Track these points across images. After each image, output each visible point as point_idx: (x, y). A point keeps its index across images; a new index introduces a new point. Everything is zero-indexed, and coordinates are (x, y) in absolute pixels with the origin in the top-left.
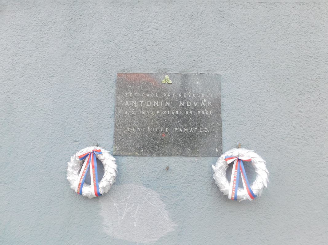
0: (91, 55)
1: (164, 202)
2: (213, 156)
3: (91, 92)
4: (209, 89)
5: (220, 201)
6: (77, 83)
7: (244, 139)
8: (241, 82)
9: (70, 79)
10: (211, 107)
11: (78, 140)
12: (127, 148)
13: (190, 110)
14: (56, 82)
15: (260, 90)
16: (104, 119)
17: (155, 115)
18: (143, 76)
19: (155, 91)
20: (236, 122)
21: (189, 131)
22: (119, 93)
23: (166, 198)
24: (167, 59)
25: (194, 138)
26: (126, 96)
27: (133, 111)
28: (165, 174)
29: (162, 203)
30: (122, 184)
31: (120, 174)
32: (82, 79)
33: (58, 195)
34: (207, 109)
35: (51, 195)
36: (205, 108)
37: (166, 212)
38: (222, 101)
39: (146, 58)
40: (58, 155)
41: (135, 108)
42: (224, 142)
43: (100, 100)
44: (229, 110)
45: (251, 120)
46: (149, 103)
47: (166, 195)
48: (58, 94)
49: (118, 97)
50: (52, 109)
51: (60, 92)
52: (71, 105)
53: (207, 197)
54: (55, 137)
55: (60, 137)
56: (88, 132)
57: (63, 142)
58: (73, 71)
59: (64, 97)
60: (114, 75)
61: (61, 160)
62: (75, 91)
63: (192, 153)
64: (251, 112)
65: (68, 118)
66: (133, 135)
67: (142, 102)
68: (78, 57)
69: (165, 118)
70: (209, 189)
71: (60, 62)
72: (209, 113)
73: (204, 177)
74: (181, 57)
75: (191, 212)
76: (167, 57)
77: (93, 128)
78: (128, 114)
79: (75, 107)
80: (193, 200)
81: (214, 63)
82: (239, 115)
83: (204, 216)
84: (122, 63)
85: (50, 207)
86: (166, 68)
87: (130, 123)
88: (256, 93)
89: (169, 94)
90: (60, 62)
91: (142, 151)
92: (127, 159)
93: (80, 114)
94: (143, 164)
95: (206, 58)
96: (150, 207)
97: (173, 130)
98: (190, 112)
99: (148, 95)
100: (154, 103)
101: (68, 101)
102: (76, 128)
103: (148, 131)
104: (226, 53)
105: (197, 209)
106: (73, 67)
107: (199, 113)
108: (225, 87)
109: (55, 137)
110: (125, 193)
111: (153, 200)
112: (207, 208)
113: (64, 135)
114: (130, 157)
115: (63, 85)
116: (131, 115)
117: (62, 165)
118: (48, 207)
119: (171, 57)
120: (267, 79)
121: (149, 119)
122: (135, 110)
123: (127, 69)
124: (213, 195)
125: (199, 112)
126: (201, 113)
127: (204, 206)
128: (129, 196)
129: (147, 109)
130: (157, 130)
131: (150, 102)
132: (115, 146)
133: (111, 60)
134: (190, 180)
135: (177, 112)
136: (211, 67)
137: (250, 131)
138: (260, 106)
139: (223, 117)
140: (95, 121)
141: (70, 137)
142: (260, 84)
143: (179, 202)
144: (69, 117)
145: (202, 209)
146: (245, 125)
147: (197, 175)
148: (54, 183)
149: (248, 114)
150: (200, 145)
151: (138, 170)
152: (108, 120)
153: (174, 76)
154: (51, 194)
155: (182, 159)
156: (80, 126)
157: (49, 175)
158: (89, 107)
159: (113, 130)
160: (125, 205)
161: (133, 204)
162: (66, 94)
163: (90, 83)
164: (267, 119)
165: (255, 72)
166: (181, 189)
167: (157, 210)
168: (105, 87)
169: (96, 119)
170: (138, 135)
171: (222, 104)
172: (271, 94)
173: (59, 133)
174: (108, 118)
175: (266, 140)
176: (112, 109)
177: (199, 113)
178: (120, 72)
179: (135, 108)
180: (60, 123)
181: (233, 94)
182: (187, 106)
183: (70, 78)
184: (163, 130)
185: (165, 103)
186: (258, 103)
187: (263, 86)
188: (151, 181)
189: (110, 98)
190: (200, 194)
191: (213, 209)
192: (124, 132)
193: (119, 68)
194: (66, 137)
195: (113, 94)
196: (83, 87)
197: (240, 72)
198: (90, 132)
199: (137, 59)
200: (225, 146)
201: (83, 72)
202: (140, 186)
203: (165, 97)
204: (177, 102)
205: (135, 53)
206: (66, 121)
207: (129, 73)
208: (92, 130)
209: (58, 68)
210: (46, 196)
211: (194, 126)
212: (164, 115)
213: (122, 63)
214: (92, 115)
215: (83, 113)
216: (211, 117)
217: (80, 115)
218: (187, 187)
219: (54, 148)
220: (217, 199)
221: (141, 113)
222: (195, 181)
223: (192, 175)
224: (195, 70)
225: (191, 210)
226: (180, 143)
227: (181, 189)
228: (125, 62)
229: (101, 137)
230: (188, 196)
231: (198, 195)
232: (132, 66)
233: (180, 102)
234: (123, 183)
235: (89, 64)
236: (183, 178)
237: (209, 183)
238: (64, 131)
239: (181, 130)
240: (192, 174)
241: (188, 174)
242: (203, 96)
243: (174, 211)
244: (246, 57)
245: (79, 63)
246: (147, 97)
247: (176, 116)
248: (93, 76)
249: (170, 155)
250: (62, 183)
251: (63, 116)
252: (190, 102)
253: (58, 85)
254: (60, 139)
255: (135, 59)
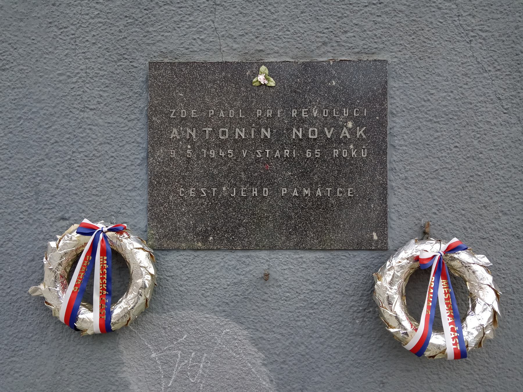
0: (87, 17)
1: (258, 349)
2: (367, 250)
3: (92, 107)
4: (361, 97)
5: (381, 347)
6: (58, 86)
7: (437, 213)
8: (438, 78)
9: (41, 77)
10: (363, 140)
11: (67, 216)
12: (179, 233)
13: (317, 146)
14: (9, 84)
15: (481, 96)
16: (125, 168)
17: (237, 158)
18: (209, 69)
19: (238, 104)
20: (421, 173)
21: (313, 194)
22: (156, 110)
23: (265, 339)
24: (265, 27)
25: (324, 209)
26: (172, 116)
27: (188, 152)
28: (262, 288)
29: (256, 350)
30: (168, 311)
31: (164, 290)
32: (68, 76)
33: (30, 335)
34: (354, 145)
35: (15, 335)
36: (350, 141)
37: (263, 369)
38: (390, 124)
39: (216, 24)
40: (24, 249)
41: (193, 144)
42: (392, 219)
43: (114, 125)
44: (406, 146)
45: (457, 167)
46: (224, 133)
47: (264, 333)
48: (17, 112)
49: (154, 118)
50: (4, 147)
51: (20, 107)
52: (47, 136)
53: (352, 338)
54: (15, 209)
55: (26, 209)
56: (90, 199)
57: (34, 221)
58: (47, 56)
59: (31, 119)
60: (142, 66)
61: (33, 260)
62: (53, 105)
63: (320, 242)
64: (458, 149)
65: (41, 167)
66: (191, 204)
67: (208, 130)
68: (56, 23)
69: (261, 166)
70: (357, 321)
71: (16, 36)
72: (358, 153)
73: (345, 294)
74: (297, 20)
75: (317, 369)
76: (264, 20)
77: (100, 189)
78: (178, 159)
79: (56, 142)
80: (322, 343)
81: (375, 32)
82: (427, 157)
83: (345, 379)
84: (160, 37)
85: (15, 361)
86: (262, 48)
87: (184, 178)
88: (471, 104)
89: (268, 111)
90: (16, 36)
91: (211, 238)
92: (180, 257)
93: (69, 157)
94: (214, 267)
95: (354, 21)
96: (229, 359)
97: (277, 192)
98: (316, 153)
99: (222, 114)
100: (234, 133)
101: (40, 126)
102: (62, 190)
103: (222, 195)
104: (403, 8)
105: (331, 364)
106: (46, 47)
107: (336, 153)
108: (398, 93)
109: (15, 209)
110: (176, 330)
111: (236, 345)
112: (352, 362)
113: (36, 204)
114: (185, 253)
115: (25, 90)
116: (184, 159)
117: (35, 272)
118: (10, 360)
119: (274, 20)
120: (499, 70)
121: (225, 168)
122: (193, 148)
123: (171, 52)
124: (365, 334)
125: (336, 152)
126: (340, 154)
127: (345, 358)
128: (185, 337)
129: (220, 147)
130: (242, 193)
131: (227, 130)
132: (151, 229)
133: (134, 30)
134: (315, 301)
135: (287, 153)
136: (366, 44)
137: (453, 194)
138: (479, 136)
139: (390, 162)
140: (104, 173)
141: (49, 209)
142: (481, 82)
143: (291, 348)
144: (45, 164)
145: (340, 363)
146: (442, 181)
147: (330, 290)
148: (20, 311)
149: (448, 154)
150: (338, 225)
151: (204, 281)
152: (134, 172)
153: (280, 67)
154: (15, 333)
155: (297, 256)
156: (71, 184)
157: (8, 293)
158: (89, 141)
159: (146, 192)
160: (176, 356)
161: (193, 354)
162: (34, 112)
163: (88, 85)
164: (493, 164)
165: (471, 54)
166: (297, 321)
167: (244, 366)
168: (122, 94)
169: (106, 170)
170: (202, 204)
171: (388, 132)
172: (506, 107)
173: (22, 201)
174: (133, 167)
175: (488, 212)
176: (141, 146)
177: (336, 153)
178: (159, 59)
179: (193, 144)
180: (26, 178)
181: (417, 109)
182: (308, 138)
183: (41, 74)
184: (256, 193)
185: (258, 132)
186: (474, 128)
187: (487, 86)
188: (232, 304)
189: (135, 122)
190: (337, 332)
191: (365, 364)
192: (171, 198)
193: (154, 48)
194: (40, 210)
195: (141, 110)
196: (73, 94)
197: (435, 55)
198: (94, 197)
199: (194, 27)
200: (393, 226)
201: (71, 60)
202: (208, 316)
203: (259, 118)
204: (287, 130)
205: (189, 13)
206: (37, 174)
207: (177, 61)
208: (97, 193)
209: (12, 50)
210: (4, 338)
211: (324, 183)
212: (257, 160)
213: (160, 37)
214: (98, 160)
215: (75, 154)
216: (364, 162)
217: (70, 159)
218: (308, 317)
219: (15, 235)
220: (373, 344)
221: (208, 155)
222: (325, 303)
223: (320, 291)
224: (330, 52)
225: (317, 367)
226: (293, 222)
227: (297, 321)
228: (167, 34)
229: (120, 208)
230: (311, 336)
231: (334, 334)
232: (183, 43)
233: (295, 130)
234: (172, 309)
235: (84, 40)
236: (299, 298)
237: (356, 308)
238: (35, 197)
239: (295, 193)
240: (319, 289)
241: (311, 287)
242: (346, 113)
243: (282, 368)
244: (450, 17)
245: (60, 37)
246: (221, 119)
247: (285, 161)
248: (93, 69)
249: (272, 248)
250: (37, 309)
251: (31, 161)
252: (316, 129)
253: (16, 90)
254: (26, 213)
255: (190, 27)
